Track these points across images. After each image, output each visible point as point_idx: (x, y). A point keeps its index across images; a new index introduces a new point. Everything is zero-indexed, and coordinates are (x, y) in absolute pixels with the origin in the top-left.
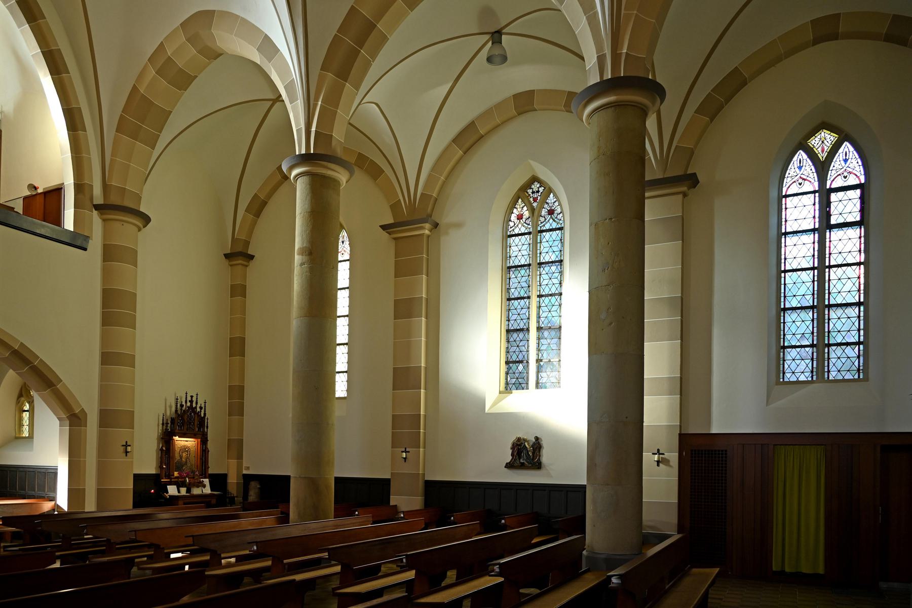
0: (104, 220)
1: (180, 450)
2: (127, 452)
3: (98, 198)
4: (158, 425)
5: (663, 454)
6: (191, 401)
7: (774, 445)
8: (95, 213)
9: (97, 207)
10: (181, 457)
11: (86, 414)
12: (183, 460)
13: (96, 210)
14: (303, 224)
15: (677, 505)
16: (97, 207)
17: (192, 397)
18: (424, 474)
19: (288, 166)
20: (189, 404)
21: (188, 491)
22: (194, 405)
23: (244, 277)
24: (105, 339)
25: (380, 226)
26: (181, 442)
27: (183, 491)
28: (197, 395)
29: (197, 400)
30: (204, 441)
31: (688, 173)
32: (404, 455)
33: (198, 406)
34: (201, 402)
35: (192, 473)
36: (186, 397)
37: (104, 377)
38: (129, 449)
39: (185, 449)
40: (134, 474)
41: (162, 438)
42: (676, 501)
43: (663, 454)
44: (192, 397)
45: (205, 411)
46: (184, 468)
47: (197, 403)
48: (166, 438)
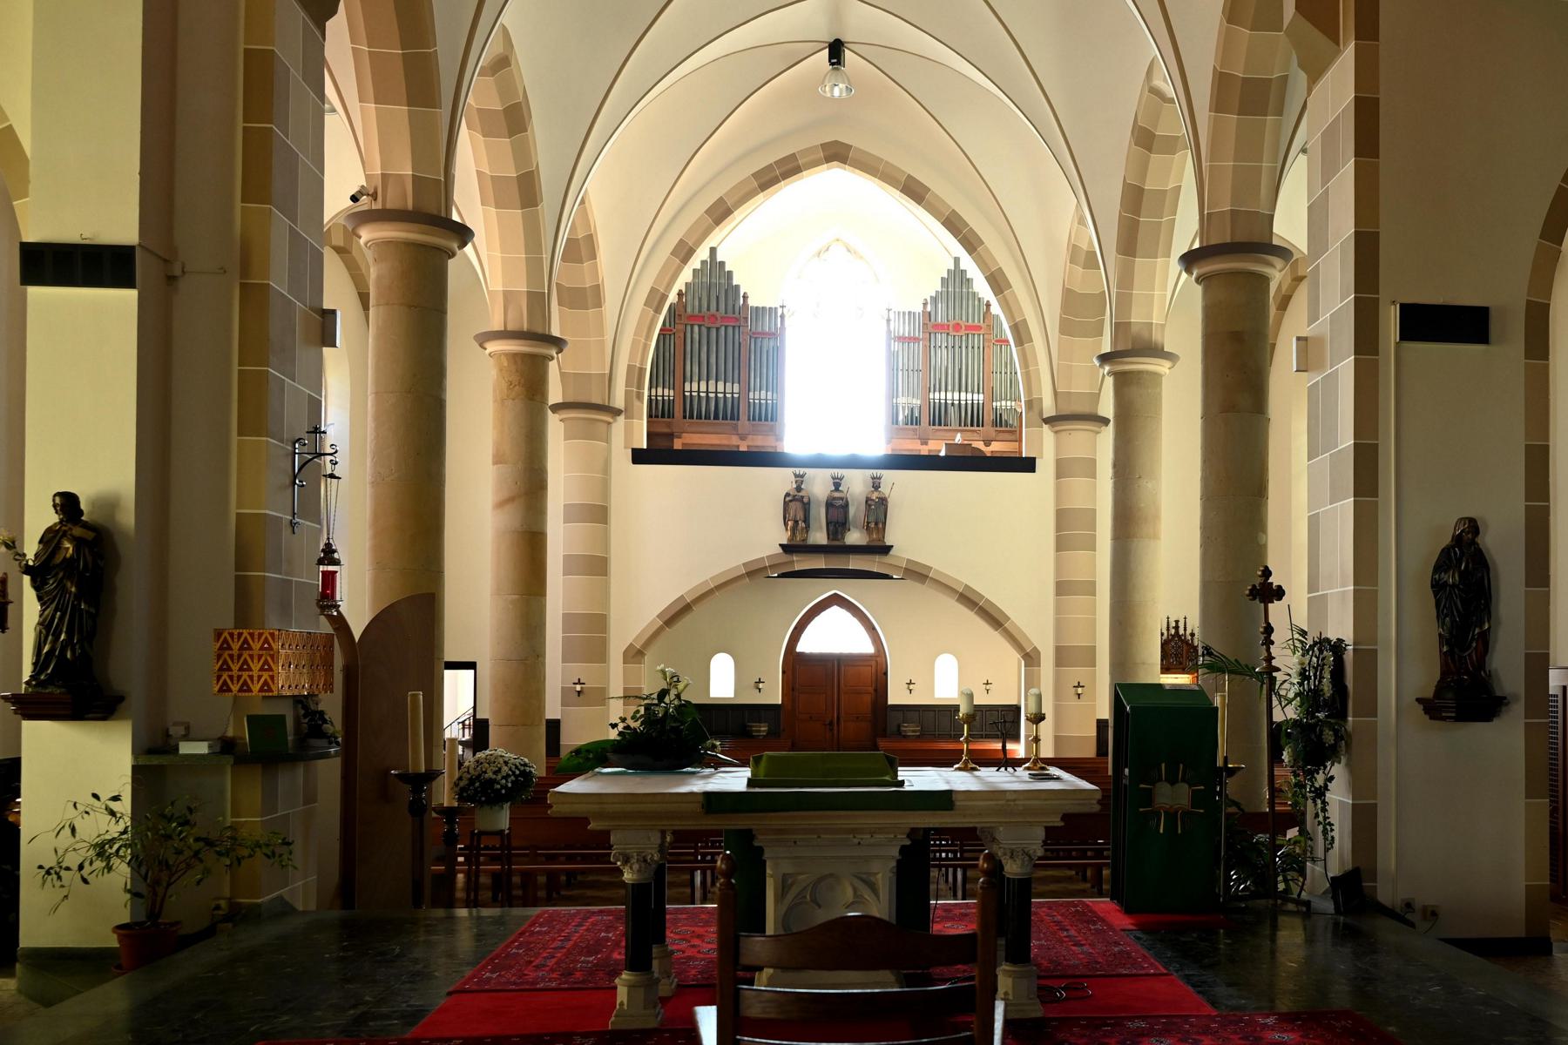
0: (1056, 432)
2: (760, 689)
3: (1049, 409)
5: (584, 684)
6: (1177, 628)
8: (1046, 427)
9: (1047, 421)
11: (1039, 653)
13: (1046, 424)
15: (1095, 739)
16: (1047, 421)
17: (1177, 622)
19: (890, 453)
20: (1173, 631)
22: (1181, 631)
24: (1059, 566)
25: (780, 545)
29: (1185, 625)
32: (578, 688)
33: (1188, 632)
37: (1058, 610)
38: (761, 685)
40: (1098, 720)
42: (1095, 734)
43: (584, 684)
44: (1177, 622)
47: (1185, 629)
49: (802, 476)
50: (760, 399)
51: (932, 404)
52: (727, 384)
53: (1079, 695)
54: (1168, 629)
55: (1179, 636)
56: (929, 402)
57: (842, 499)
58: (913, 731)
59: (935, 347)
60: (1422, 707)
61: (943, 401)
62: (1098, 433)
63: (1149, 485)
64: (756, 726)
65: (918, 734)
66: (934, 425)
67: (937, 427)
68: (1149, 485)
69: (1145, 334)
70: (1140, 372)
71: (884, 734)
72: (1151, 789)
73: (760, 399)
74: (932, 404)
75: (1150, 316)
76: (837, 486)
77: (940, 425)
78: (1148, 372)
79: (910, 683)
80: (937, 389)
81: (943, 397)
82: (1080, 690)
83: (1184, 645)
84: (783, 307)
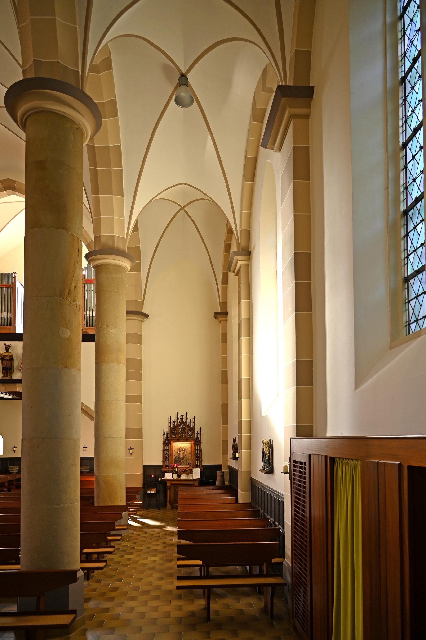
1: (178, 450)
4: (164, 435)
6: (182, 419)
7: (169, 618)
10: (179, 455)
12: (181, 456)
14: (6, 384)
18: (250, 472)
20: (180, 420)
21: (179, 476)
23: (140, 351)
26: (178, 445)
27: (175, 476)
28: (187, 414)
30: (198, 442)
31: (5, 106)
34: (190, 418)
35: (188, 465)
36: (178, 416)
39: (182, 449)
40: (81, 457)
41: (163, 443)
44: (182, 416)
45: (194, 424)
46: (181, 461)
47: (187, 420)
48: (167, 442)
49: (10, 346)
50: (4, 316)
51: (86, 317)
52: (8, 313)
53: (131, 453)
54: (178, 420)
55: (184, 423)
56: (84, 316)
57: (10, 356)
58: (85, 469)
59: (87, 290)
60: (102, 566)
61: (91, 316)
62: (142, 322)
63: (114, 331)
64: (11, 468)
65: (88, 470)
66: (87, 326)
67: (88, 328)
68: (114, 331)
69: (110, 243)
70: (107, 265)
71: (196, 445)
72: (214, 483)
73: (4, 316)
74: (86, 317)
75: (112, 230)
76: (7, 350)
77: (90, 326)
78: (112, 265)
79: (85, 447)
80: (91, 309)
81: (91, 313)
82: (131, 451)
83: (186, 427)
84: (15, 273)
